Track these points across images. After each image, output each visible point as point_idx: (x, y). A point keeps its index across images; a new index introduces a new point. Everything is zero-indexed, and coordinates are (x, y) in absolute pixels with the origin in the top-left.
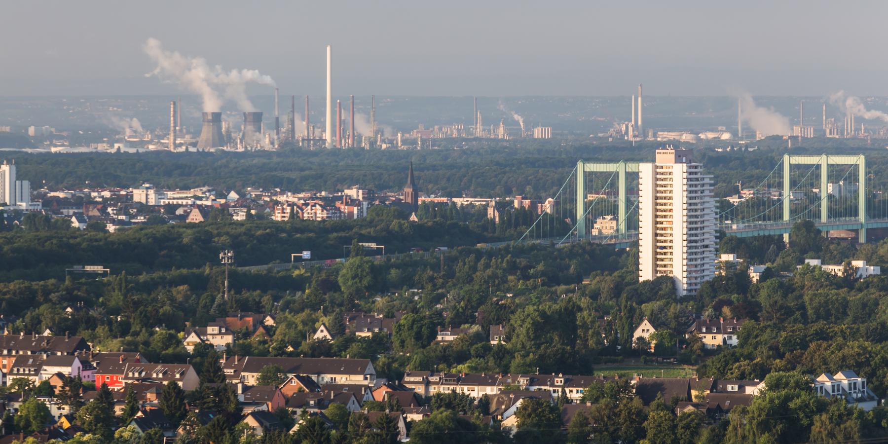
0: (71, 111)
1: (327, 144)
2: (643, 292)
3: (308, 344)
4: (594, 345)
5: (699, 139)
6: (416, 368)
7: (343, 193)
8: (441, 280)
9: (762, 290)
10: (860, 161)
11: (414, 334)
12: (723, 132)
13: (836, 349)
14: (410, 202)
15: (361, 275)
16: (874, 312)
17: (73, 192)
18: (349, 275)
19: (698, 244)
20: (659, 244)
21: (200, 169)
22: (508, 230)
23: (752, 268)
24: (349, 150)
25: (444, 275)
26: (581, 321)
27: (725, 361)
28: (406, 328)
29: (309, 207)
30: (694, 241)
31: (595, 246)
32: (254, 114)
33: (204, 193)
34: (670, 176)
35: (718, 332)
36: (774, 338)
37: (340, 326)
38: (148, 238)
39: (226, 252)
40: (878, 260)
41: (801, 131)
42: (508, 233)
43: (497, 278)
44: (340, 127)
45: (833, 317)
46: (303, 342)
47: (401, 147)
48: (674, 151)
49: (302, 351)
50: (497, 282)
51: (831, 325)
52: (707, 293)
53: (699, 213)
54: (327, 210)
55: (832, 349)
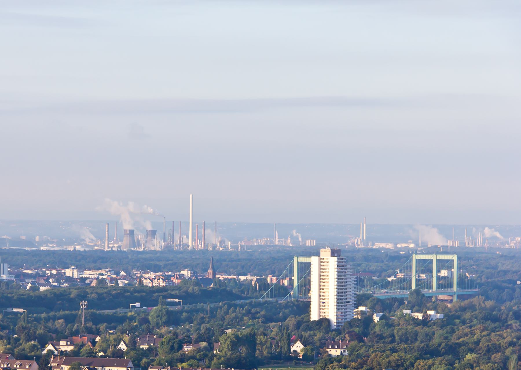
0: (64, 229)
1: (189, 248)
2: (312, 327)
3: (111, 351)
4: (266, 354)
5: (396, 247)
6: (157, 364)
7: (180, 273)
8: (207, 319)
9: (377, 326)
10: (454, 258)
11: (169, 347)
12: (411, 243)
13: (386, 357)
14: (211, 278)
15: (162, 315)
16: (432, 339)
17: (36, 270)
18: (155, 316)
19: (343, 301)
20: (322, 301)
21: (112, 259)
22: (255, 293)
23: (375, 314)
24: (201, 250)
25: (209, 316)
26: (259, 341)
27: (325, 363)
28: (166, 343)
29: (156, 280)
30: (341, 299)
31: (300, 302)
32: (152, 230)
33: (107, 272)
34: (328, 264)
35: (338, 348)
36: (367, 352)
37: (133, 342)
38: (51, 295)
39: (84, 301)
40: (448, 311)
41: (452, 243)
42: (255, 295)
43: (238, 318)
44: (197, 237)
45: (410, 341)
46: (108, 350)
47: (230, 249)
48: (330, 250)
49: (107, 355)
50: (238, 320)
51: (399, 345)
52: (347, 328)
53: (343, 284)
54: (165, 282)
55: (383, 357)
